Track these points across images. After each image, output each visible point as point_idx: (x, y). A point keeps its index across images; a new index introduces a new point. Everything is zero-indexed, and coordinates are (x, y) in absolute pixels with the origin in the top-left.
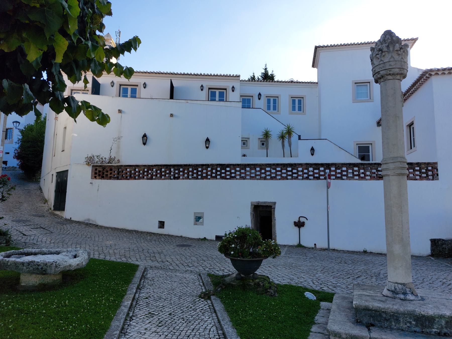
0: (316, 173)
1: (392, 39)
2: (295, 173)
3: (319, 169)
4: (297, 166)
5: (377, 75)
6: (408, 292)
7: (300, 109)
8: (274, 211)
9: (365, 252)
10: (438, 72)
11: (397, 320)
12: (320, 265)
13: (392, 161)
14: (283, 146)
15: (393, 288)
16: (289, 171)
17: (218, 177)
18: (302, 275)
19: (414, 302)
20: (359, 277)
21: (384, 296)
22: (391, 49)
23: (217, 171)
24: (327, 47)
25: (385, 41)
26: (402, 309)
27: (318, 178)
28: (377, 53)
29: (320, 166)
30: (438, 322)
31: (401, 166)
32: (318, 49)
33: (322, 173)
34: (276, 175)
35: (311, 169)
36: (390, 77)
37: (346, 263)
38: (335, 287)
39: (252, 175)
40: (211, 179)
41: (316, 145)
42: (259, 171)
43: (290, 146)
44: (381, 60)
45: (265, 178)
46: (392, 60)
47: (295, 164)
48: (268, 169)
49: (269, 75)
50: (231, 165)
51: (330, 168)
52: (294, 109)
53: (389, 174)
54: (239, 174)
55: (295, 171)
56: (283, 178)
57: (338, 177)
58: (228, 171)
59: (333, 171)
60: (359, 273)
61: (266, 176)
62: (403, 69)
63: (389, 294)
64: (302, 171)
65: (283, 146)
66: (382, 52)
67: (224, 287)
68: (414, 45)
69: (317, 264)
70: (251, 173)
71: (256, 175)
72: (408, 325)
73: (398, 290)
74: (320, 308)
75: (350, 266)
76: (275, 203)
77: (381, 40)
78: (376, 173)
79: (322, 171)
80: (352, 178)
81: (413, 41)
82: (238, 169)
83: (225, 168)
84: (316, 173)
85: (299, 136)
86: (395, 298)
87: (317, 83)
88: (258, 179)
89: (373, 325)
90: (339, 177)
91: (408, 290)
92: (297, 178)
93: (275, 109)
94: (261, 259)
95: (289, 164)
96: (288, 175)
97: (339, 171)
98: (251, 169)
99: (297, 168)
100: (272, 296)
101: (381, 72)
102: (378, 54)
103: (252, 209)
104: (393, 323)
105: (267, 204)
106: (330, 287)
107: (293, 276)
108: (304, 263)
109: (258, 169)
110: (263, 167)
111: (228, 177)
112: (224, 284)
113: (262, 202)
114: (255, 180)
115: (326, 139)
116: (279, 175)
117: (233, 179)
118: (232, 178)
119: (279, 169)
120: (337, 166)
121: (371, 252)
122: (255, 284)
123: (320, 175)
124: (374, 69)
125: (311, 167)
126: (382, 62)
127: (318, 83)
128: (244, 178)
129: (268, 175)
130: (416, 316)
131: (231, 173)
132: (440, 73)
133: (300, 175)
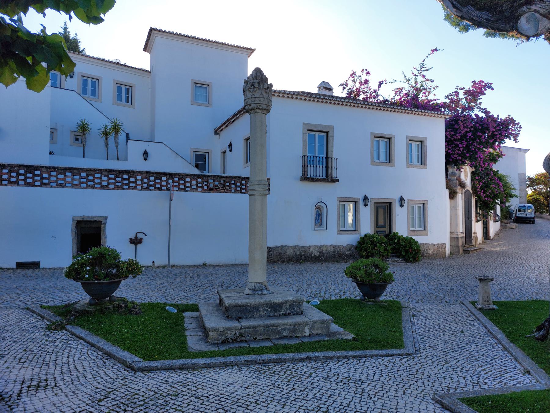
0: (158, 183)
1: (262, 77)
2: (132, 182)
3: (161, 179)
4: (136, 174)
5: (248, 106)
6: (264, 289)
7: (127, 100)
8: (105, 227)
9: (205, 265)
10: (275, 94)
11: (258, 310)
12: (166, 282)
13: (258, 184)
14: (107, 145)
15: (253, 287)
16: (126, 179)
17: (21, 183)
18: (152, 293)
19: (268, 295)
20: (207, 288)
21: (246, 294)
22: (261, 87)
23: (19, 174)
24: (164, 32)
25: (256, 78)
26: (262, 301)
27: (160, 189)
28: (250, 87)
29: (162, 176)
30: (285, 306)
31: (264, 188)
32: (153, 31)
33: (164, 183)
34: (109, 184)
35: (152, 178)
36: (259, 111)
37: (190, 277)
38: (188, 300)
39: (75, 182)
40: (8, 185)
41: (150, 148)
42: (85, 178)
43: (117, 145)
44: (253, 94)
45: (93, 187)
46: (261, 96)
47: (133, 172)
48: (97, 175)
49: (71, 38)
50: (42, 167)
51: (174, 179)
52: (119, 98)
53: (255, 193)
54: (55, 181)
55: (132, 180)
56: (117, 188)
57: (182, 188)
58: (38, 175)
59: (177, 182)
60: (206, 284)
61: (95, 184)
62: (269, 106)
63: (250, 292)
64: (142, 180)
65: (107, 145)
66: (254, 87)
67: (78, 315)
68: (252, 55)
69: (163, 281)
70: (73, 180)
71: (82, 183)
72: (266, 312)
73: (257, 288)
74: (184, 318)
75: (196, 279)
76: (106, 218)
77: (254, 76)
78: (219, 186)
79: (165, 181)
80: (196, 190)
81: (251, 51)
82: (53, 173)
83: (32, 171)
84: (158, 183)
85: (128, 135)
86: (254, 295)
87: (150, 72)
88: (83, 188)
89: (240, 318)
90: (182, 189)
91: (264, 287)
92: (135, 188)
93: (93, 93)
94: (120, 279)
95: (125, 171)
96: (123, 184)
97: (182, 182)
98: (74, 174)
99: (136, 176)
100: (137, 314)
101: (252, 105)
102: (251, 88)
103: (75, 225)
104: (255, 313)
105: (95, 219)
106: (184, 300)
107: (143, 296)
108: (149, 282)
109: (84, 175)
110: (92, 173)
111: (36, 183)
112: (76, 312)
113: (89, 217)
114: (79, 188)
115: (162, 143)
116: (112, 184)
117: (46, 186)
118: (43, 185)
119: (112, 176)
120: (181, 176)
121: (210, 265)
122: (114, 307)
123: (162, 186)
124: (246, 101)
125: (151, 176)
126: (253, 96)
127: (151, 72)
128: (62, 186)
129: (98, 184)
130: (272, 304)
131: (43, 179)
132: (276, 94)
133: (139, 185)
